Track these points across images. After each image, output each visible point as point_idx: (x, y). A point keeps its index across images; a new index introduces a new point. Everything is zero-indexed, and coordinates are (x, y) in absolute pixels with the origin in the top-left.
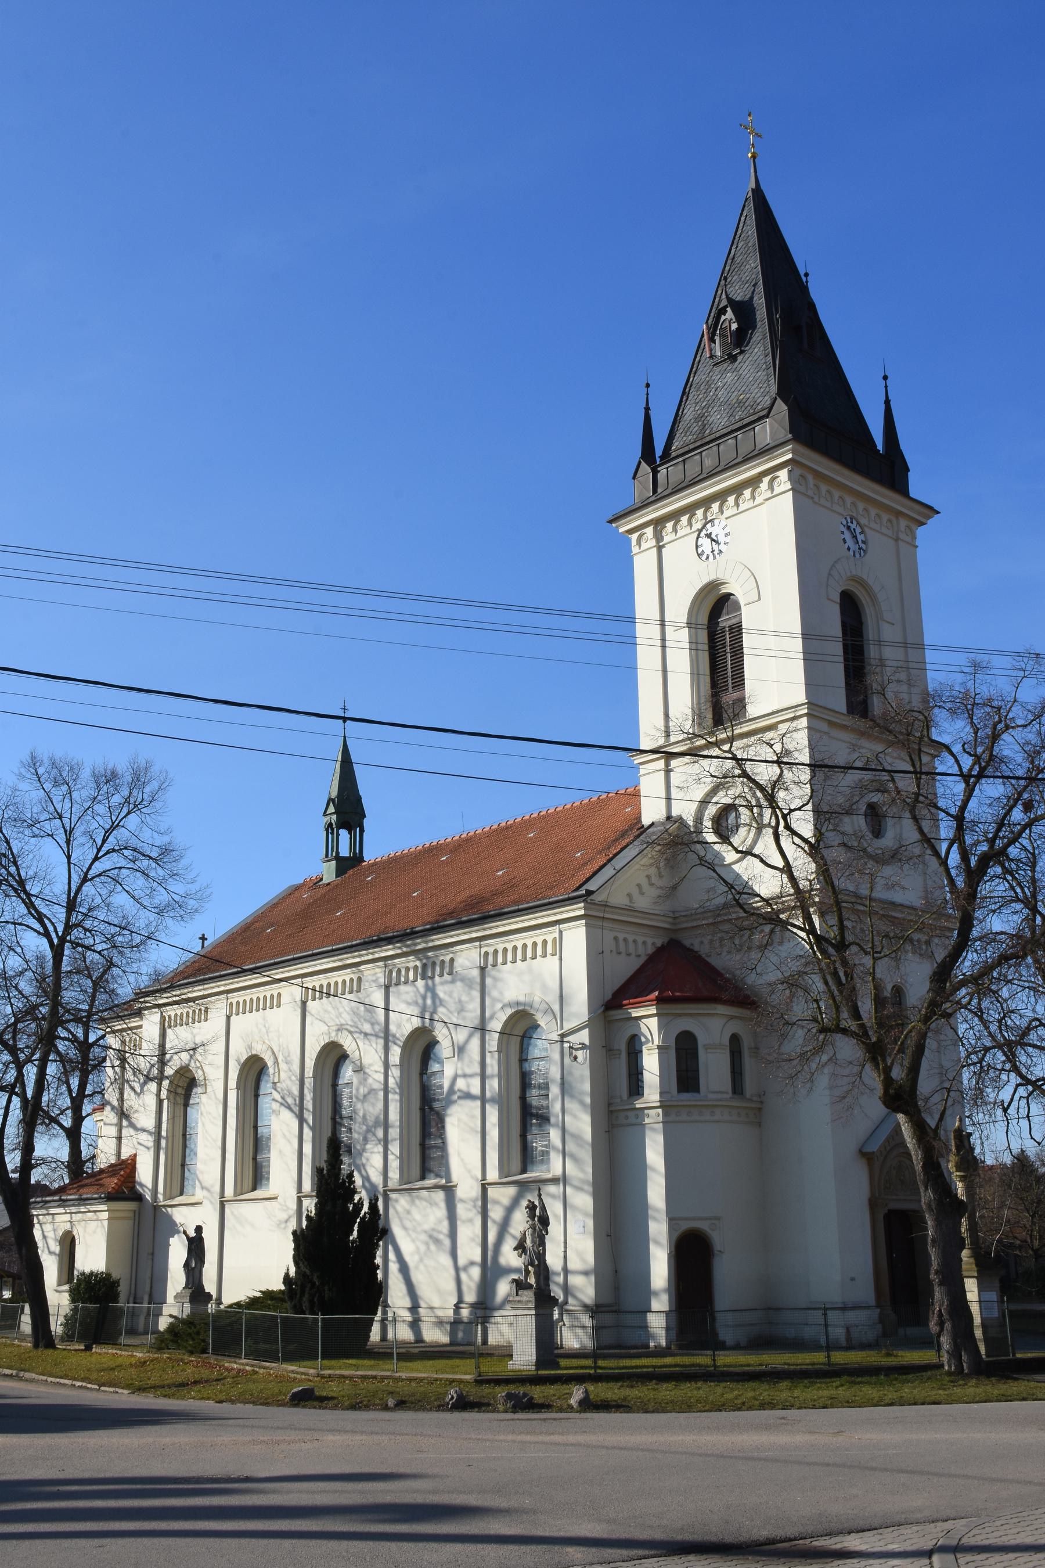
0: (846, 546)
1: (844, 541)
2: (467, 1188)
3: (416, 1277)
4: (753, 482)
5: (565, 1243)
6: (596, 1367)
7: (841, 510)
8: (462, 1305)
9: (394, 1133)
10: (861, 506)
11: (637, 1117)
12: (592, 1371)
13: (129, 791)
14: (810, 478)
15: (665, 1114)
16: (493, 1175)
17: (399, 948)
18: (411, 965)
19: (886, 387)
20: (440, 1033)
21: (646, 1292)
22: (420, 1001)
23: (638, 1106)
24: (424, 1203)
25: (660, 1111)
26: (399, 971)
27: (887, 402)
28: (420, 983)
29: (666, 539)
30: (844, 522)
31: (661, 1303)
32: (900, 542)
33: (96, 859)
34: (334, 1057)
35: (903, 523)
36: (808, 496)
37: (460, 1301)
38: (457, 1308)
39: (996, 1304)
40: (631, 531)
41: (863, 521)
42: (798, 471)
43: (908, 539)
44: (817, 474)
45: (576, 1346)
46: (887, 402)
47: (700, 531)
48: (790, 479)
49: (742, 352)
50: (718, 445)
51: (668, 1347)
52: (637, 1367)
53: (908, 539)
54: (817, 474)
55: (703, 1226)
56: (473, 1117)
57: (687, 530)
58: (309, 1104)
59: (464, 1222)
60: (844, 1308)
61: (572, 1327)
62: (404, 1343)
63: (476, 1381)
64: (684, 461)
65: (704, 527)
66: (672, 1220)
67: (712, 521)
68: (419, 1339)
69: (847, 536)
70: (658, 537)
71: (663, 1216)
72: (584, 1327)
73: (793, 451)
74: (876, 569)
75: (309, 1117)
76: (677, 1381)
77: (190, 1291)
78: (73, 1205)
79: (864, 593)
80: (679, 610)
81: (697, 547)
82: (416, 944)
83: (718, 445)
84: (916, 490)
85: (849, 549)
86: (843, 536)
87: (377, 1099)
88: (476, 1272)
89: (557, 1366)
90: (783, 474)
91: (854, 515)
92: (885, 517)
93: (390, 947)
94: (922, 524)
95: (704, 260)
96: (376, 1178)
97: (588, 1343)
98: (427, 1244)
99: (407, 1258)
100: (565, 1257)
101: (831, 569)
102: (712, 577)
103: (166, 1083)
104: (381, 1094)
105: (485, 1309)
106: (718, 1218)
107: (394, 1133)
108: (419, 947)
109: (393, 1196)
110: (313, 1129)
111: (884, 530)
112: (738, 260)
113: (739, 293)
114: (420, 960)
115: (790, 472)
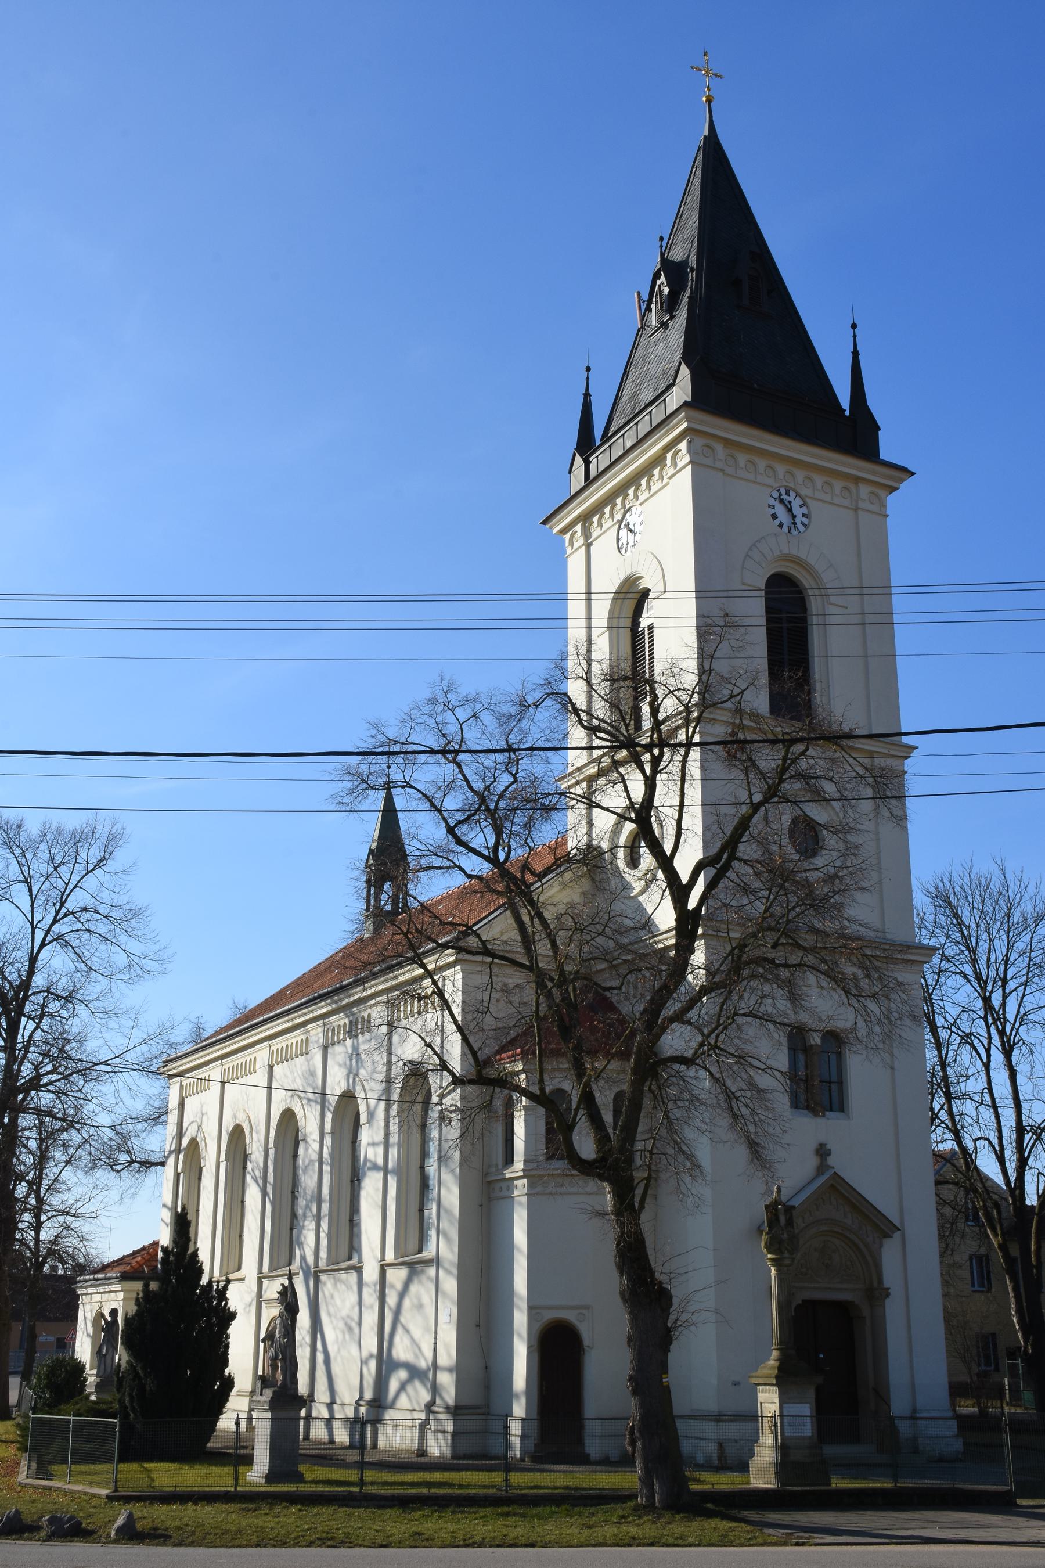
0: (777, 522)
1: (774, 516)
2: (370, 1273)
3: (336, 1369)
4: (659, 460)
5: (436, 1333)
6: (362, 1483)
7: (770, 481)
8: (361, 1403)
9: (325, 1208)
10: (800, 475)
11: (508, 1188)
12: (356, 1489)
13: (83, 849)
14: (719, 448)
15: (531, 1185)
16: (390, 1256)
17: (330, 1004)
18: (342, 1023)
19: (855, 336)
20: (359, 1093)
22: (348, 1063)
23: (507, 1176)
24: (343, 1287)
25: (525, 1181)
26: (333, 1030)
27: (856, 354)
28: (349, 1042)
29: (594, 535)
30: (776, 494)
31: (519, 1409)
32: (860, 512)
33: (55, 921)
34: (288, 1116)
35: (864, 490)
36: (717, 469)
37: (361, 1398)
38: (358, 1404)
39: (808, 1420)
40: (564, 531)
41: (804, 492)
42: (700, 442)
43: (875, 508)
44: (727, 443)
45: (437, 1453)
46: (856, 354)
47: (620, 522)
48: (689, 451)
49: (671, 318)
50: (637, 424)
51: (522, 1460)
53: (875, 508)
54: (727, 443)
55: (570, 1316)
56: (377, 1190)
57: (610, 523)
58: (270, 1178)
59: (367, 1308)
60: (719, 1418)
61: (437, 1431)
62: (320, 1443)
63: (110, 1498)
64: (610, 446)
65: (623, 517)
67: (630, 509)
68: (422, 1452)
69: (780, 510)
70: (587, 534)
71: (524, 1305)
72: (444, 1432)
73: (688, 418)
74: (822, 549)
75: (270, 1190)
76: (303, 1504)
77: (98, 1380)
78: (91, 1286)
79: (804, 573)
80: (602, 609)
81: (618, 540)
82: (341, 1000)
83: (637, 424)
84: (886, 453)
85: (781, 525)
86: (772, 511)
87: (313, 1170)
88: (373, 1364)
89: (299, 1478)
90: (683, 446)
91: (792, 485)
92: (838, 485)
93: (323, 1004)
94: (893, 489)
96: (310, 1259)
97: (448, 1452)
98: (344, 1333)
99: (330, 1348)
100: (435, 1350)
101: (750, 549)
102: (628, 572)
103: (181, 1156)
104: (317, 1164)
105: (379, 1407)
106: (587, 1307)
107: (325, 1208)
108: (344, 1003)
109: (323, 1277)
110: (273, 1203)
111: (836, 500)
112: (684, 217)
113: (677, 255)
114: (348, 1017)
115: (689, 442)
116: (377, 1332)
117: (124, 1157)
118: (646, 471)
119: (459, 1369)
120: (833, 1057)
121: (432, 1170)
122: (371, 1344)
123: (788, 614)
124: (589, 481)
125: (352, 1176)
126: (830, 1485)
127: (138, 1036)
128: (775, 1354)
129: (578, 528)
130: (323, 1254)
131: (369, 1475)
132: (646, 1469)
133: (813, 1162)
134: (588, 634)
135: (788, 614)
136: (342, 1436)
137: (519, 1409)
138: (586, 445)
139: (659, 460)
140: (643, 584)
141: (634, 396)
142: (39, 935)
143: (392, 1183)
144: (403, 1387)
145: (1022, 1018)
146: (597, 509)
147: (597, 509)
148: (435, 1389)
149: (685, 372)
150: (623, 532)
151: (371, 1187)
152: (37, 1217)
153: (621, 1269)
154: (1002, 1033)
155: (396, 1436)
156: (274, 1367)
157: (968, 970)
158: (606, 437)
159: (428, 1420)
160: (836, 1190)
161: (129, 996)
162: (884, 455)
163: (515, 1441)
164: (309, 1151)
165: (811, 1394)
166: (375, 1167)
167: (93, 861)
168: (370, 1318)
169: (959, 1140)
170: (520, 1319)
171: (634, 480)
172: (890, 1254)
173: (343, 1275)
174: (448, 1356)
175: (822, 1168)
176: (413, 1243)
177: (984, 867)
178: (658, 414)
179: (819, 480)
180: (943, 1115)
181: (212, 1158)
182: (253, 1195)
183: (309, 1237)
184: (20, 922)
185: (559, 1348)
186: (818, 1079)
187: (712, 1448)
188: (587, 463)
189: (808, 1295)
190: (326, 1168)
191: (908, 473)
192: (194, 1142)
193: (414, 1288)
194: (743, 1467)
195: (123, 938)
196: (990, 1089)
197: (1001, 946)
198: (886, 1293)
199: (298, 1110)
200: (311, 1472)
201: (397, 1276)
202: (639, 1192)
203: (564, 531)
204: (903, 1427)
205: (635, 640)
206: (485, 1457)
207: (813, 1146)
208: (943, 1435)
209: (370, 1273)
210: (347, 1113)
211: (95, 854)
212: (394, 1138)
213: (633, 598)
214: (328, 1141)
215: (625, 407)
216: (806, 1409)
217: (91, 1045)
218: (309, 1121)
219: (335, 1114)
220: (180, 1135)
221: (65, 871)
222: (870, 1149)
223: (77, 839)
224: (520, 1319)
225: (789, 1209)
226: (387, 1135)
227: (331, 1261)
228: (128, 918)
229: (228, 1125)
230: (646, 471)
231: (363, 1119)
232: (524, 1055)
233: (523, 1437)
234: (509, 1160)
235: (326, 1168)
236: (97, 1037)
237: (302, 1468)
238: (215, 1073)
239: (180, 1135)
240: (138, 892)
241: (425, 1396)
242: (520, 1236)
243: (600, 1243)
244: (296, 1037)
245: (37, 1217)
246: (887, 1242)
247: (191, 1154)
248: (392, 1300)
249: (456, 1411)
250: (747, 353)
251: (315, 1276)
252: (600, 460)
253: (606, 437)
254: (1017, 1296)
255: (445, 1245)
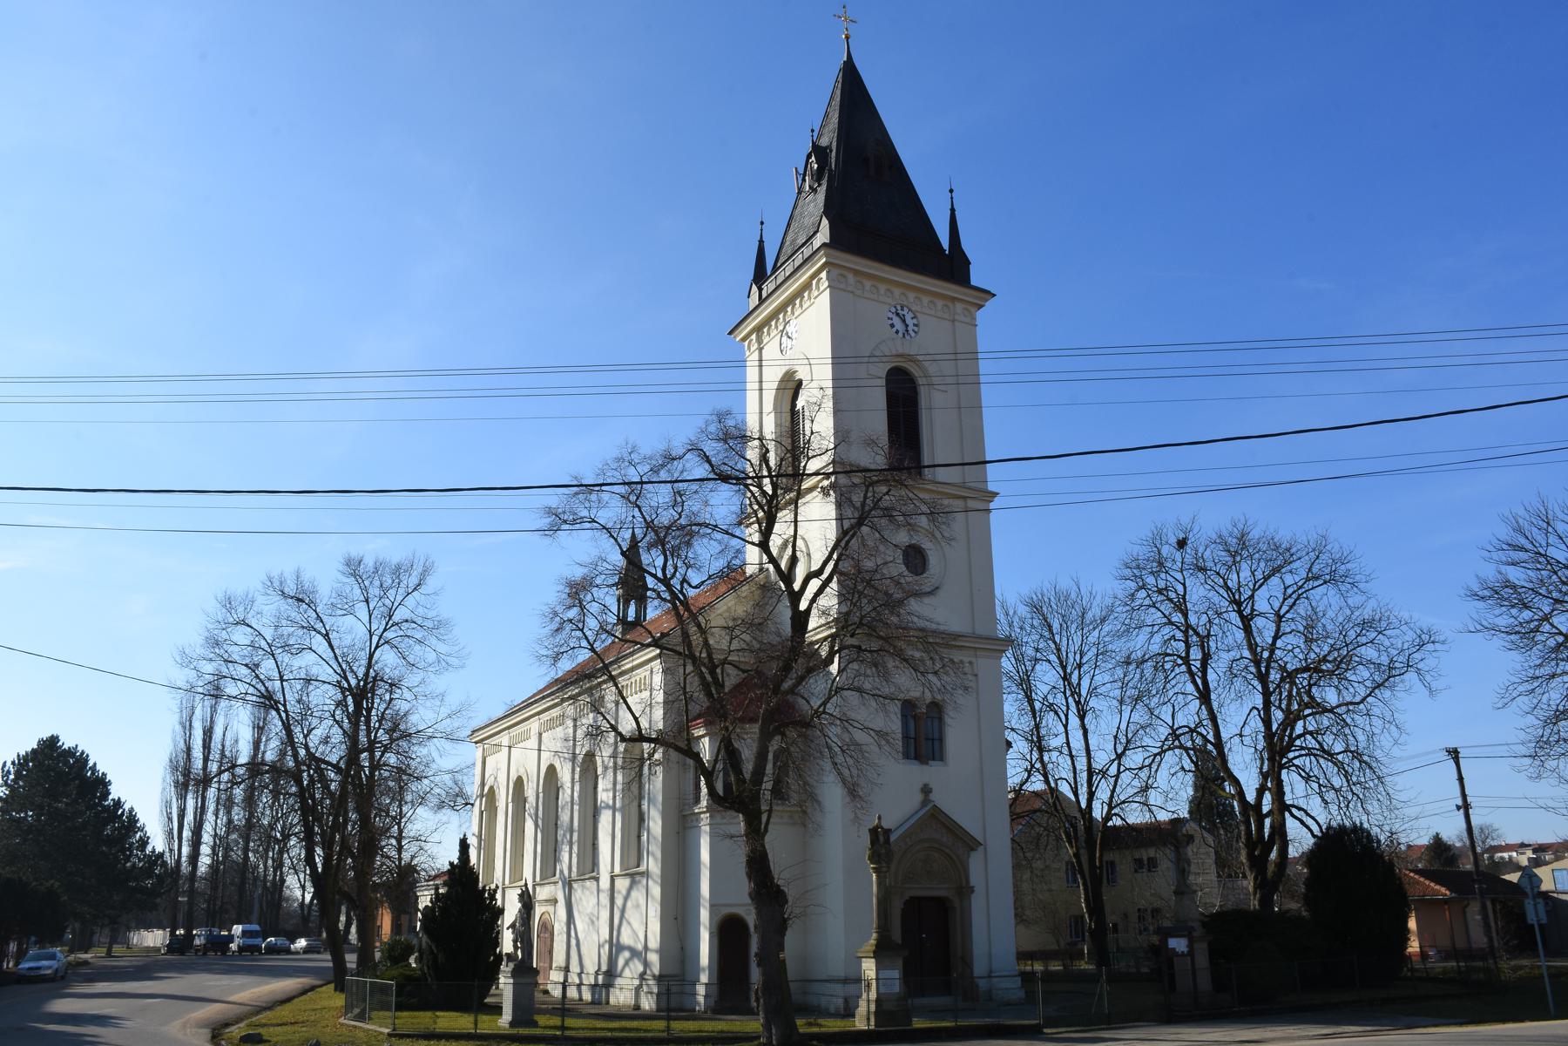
1: (892, 326)
4: (807, 286)
6: (563, 1028)
7: (889, 300)
10: (911, 296)
14: (850, 276)
16: (617, 870)
21: (697, 969)
31: (704, 978)
34: (551, 770)
35: (959, 307)
38: (597, 973)
40: (744, 339)
42: (836, 272)
43: (967, 320)
44: (856, 272)
46: (953, 210)
52: (637, 1030)
53: (967, 320)
54: (856, 272)
66: (713, 907)
68: (637, 1007)
69: (896, 321)
70: (760, 341)
89: (535, 1024)
90: (824, 275)
92: (940, 303)
95: (811, 114)
96: (566, 873)
97: (654, 1006)
109: (575, 885)
116: (602, 927)
117: (455, 800)
118: (799, 294)
119: (662, 951)
120: (936, 722)
121: (645, 807)
122: (605, 934)
123: (903, 398)
124: (762, 301)
125: (592, 812)
126: (910, 1023)
127: (444, 712)
128: (875, 935)
129: (754, 337)
130: (574, 869)
131: (570, 1022)
132: (766, 1018)
133: (919, 797)
134: (760, 416)
135: (903, 398)
136: (587, 996)
137: (704, 978)
138: (760, 276)
139: (807, 286)
140: (798, 376)
141: (793, 241)
142: (375, 639)
143: (618, 817)
144: (626, 963)
145: (1092, 691)
146: (766, 322)
147: (766, 322)
148: (646, 964)
149: (825, 222)
150: (784, 338)
151: (605, 819)
152: (399, 842)
153: (750, 878)
154: (1078, 703)
155: (621, 996)
156: (516, 948)
157: (1053, 658)
158: (775, 269)
159: (641, 986)
160: (934, 817)
161: (438, 683)
162: (973, 282)
163: (701, 999)
164: (565, 796)
165: (900, 963)
166: (608, 807)
167: (412, 586)
168: (605, 915)
169: (1047, 781)
170: (704, 915)
171: (790, 301)
172: (975, 863)
173: (588, 883)
174: (654, 943)
175: (925, 802)
176: (633, 861)
177: (1065, 584)
178: (807, 251)
179: (926, 300)
180: (1038, 765)
181: (503, 799)
182: (529, 825)
183: (565, 856)
184: (362, 631)
185: (729, 932)
186: (923, 736)
187: (840, 1002)
188: (760, 290)
189: (913, 893)
190: (576, 807)
191: (990, 294)
192: (491, 788)
193: (634, 894)
194: (849, 1013)
195: (433, 641)
196: (1068, 743)
197: (1077, 639)
198: (972, 890)
199: (558, 765)
200: (542, 1020)
201: (622, 884)
202: (764, 818)
203: (744, 339)
204: (982, 984)
205: (792, 421)
206: (682, 1010)
207: (919, 786)
208: (1011, 988)
209: (605, 882)
210: (588, 769)
211: (413, 581)
212: (619, 787)
213: (791, 387)
214: (577, 788)
215: (788, 250)
216: (896, 974)
217: (413, 718)
218: (565, 774)
219: (581, 767)
220: (483, 784)
221: (391, 593)
222: (953, 786)
223: (397, 571)
224: (704, 915)
225: (887, 832)
226: (615, 784)
227: (579, 874)
228: (438, 627)
229: (513, 777)
230: (799, 294)
231: (600, 771)
232: (706, 725)
233: (706, 997)
234: (697, 800)
235: (576, 807)
236: (420, 718)
237: (537, 1018)
238: (504, 739)
239: (483, 784)
240: (444, 608)
241: (641, 968)
242: (705, 855)
243: (739, 854)
244: (555, 712)
245: (399, 842)
246: (973, 854)
247: (490, 796)
248: (619, 902)
249: (660, 979)
250: (871, 207)
251: (568, 884)
252: (768, 287)
253: (775, 269)
254: (1086, 890)
255: (653, 864)
